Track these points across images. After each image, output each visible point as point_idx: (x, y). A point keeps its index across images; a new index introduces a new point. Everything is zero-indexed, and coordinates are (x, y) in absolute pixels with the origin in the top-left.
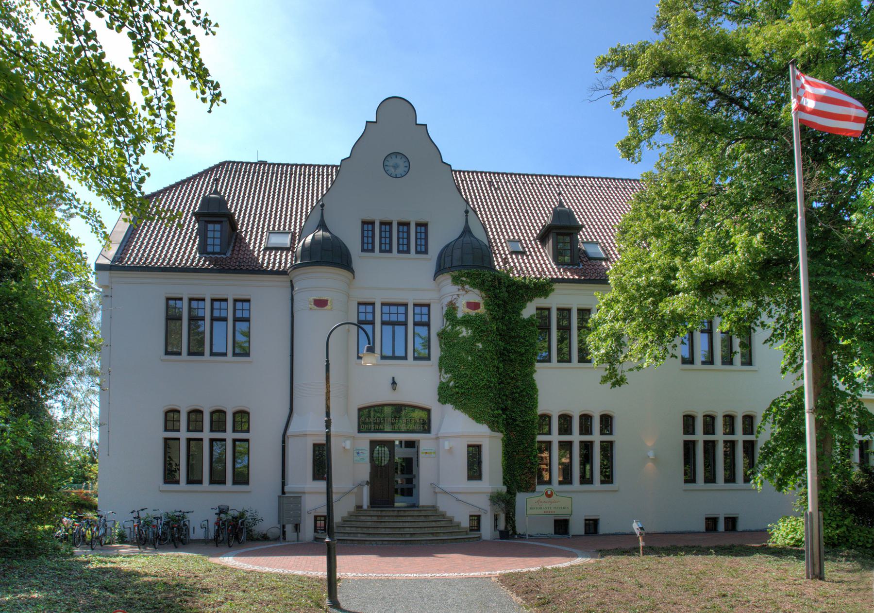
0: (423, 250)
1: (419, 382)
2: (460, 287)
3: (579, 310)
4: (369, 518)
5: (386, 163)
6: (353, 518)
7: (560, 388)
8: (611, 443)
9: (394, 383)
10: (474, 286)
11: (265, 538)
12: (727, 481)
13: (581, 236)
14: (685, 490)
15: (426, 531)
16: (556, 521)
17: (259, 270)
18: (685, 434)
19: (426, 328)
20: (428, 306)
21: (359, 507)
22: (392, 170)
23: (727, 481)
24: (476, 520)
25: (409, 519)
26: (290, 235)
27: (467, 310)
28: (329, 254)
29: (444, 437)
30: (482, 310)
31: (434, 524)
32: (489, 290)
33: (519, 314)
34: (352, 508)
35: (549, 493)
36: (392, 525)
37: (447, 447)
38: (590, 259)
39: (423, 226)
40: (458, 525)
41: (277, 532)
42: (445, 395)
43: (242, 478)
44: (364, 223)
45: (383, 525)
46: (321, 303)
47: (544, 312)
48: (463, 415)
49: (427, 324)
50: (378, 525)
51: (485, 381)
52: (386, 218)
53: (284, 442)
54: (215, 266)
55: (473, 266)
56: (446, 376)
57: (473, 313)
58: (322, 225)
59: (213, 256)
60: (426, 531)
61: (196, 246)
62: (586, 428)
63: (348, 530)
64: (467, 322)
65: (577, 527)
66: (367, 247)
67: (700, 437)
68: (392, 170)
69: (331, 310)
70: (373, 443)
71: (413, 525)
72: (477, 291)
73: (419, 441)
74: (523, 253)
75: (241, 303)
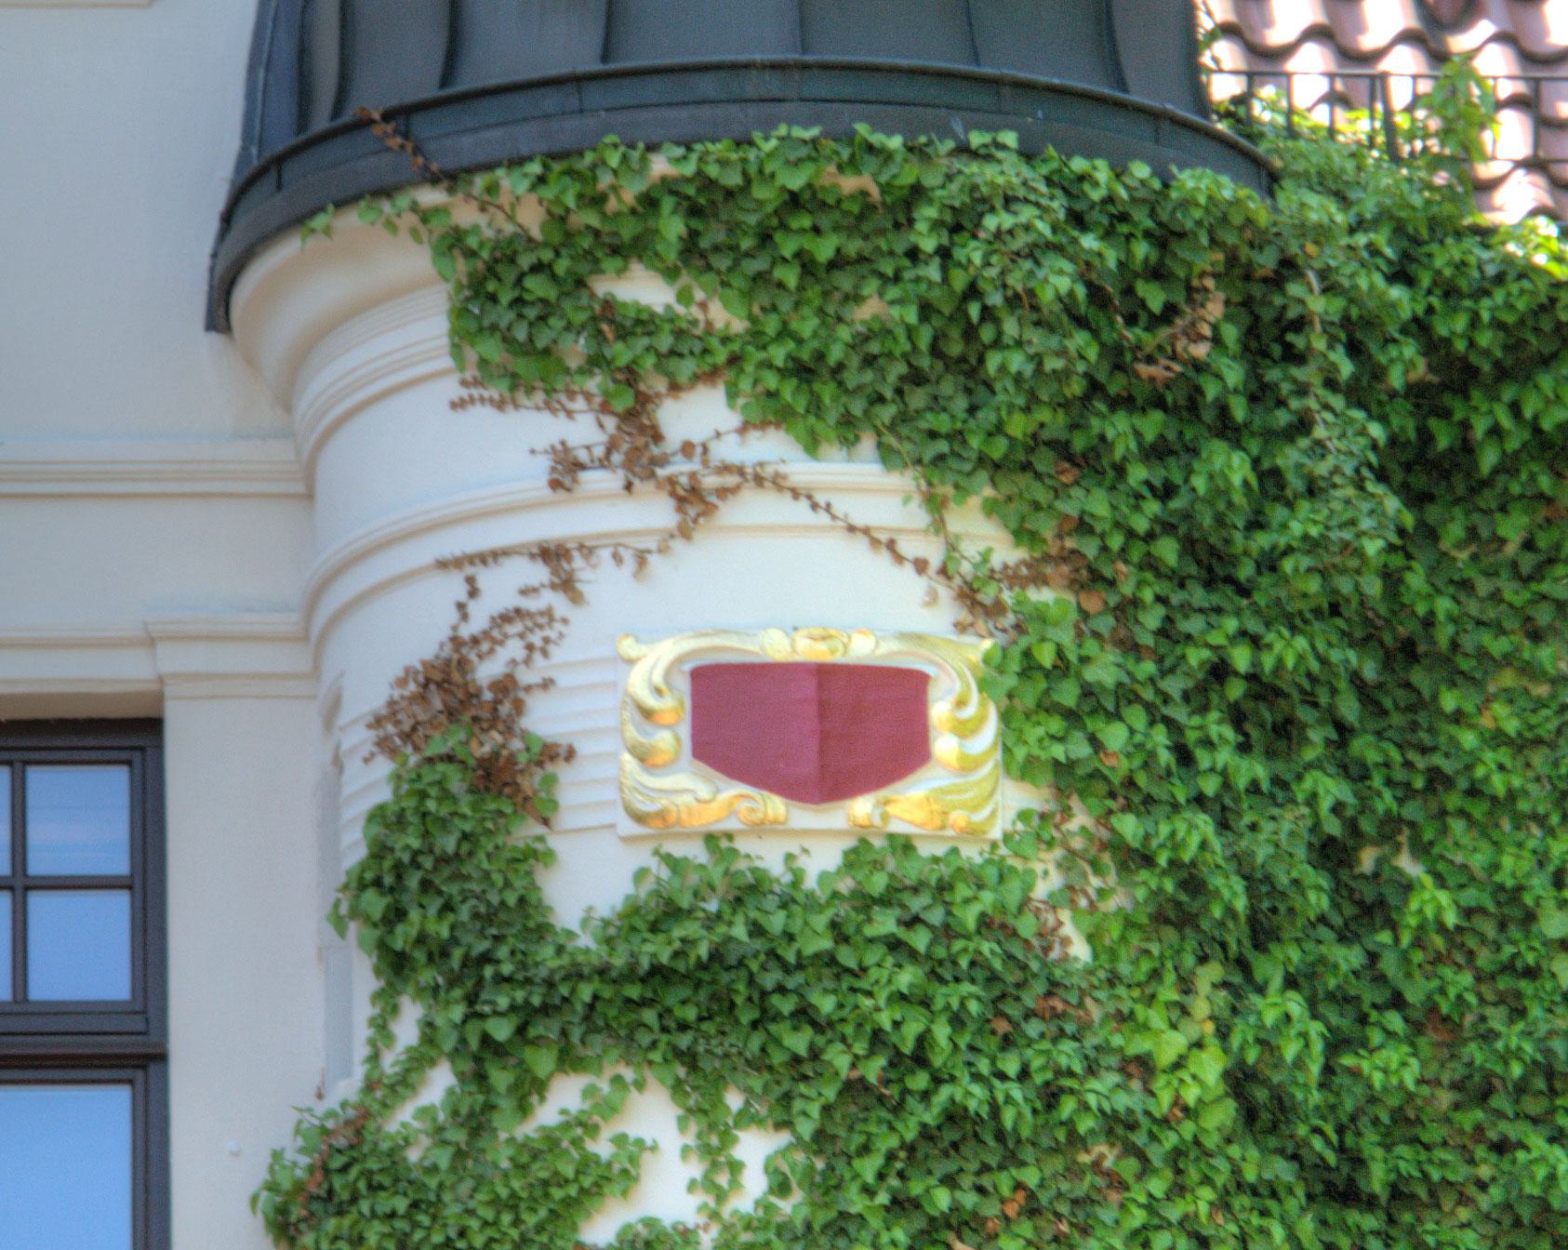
2: (584, 430)
10: (808, 391)
19: (104, 1110)
20: (126, 737)
27: (704, 798)
30: (962, 791)
55: (807, 78)
57: (806, 841)
72: (868, 484)
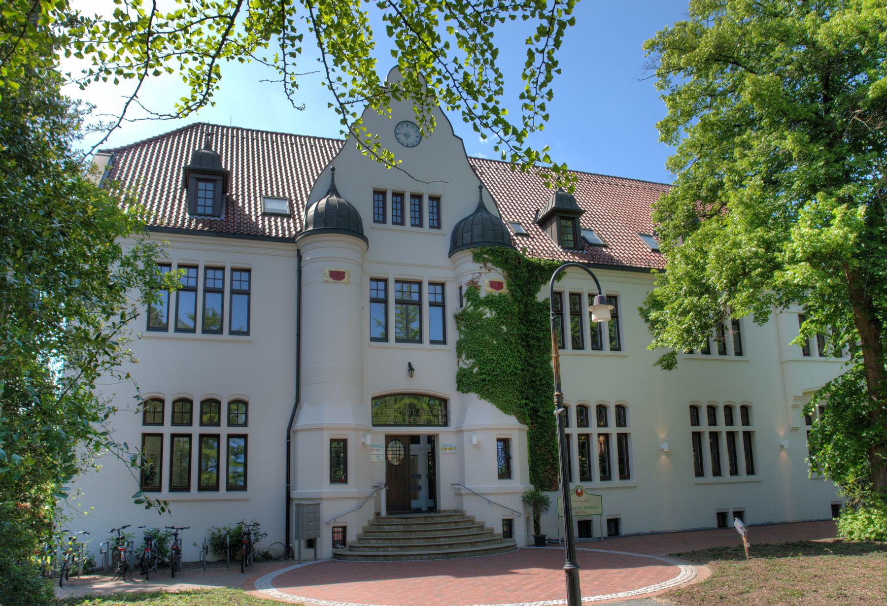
0: (437, 224)
1: (435, 368)
2: (482, 265)
3: (571, 294)
4: (394, 528)
5: (397, 131)
6: (375, 529)
7: (581, 377)
8: (626, 435)
9: (411, 368)
10: (497, 264)
11: (267, 557)
12: (602, 479)
13: (584, 221)
14: (696, 484)
15: (462, 540)
16: (718, 514)
17: (260, 236)
18: (692, 425)
21: (378, 514)
22: (403, 139)
23: (602, 479)
24: (508, 524)
25: (439, 527)
26: (287, 202)
28: (339, 221)
29: (468, 431)
30: (505, 290)
31: (466, 532)
32: (511, 269)
33: (534, 297)
34: (372, 517)
35: (579, 491)
36: (424, 535)
37: (475, 442)
38: (591, 245)
39: (436, 200)
40: (491, 532)
41: (280, 549)
42: (464, 382)
43: (239, 484)
44: (376, 192)
45: (413, 535)
46: (337, 276)
47: (557, 296)
48: (490, 404)
49: (442, 305)
50: (408, 536)
51: (512, 368)
52: (399, 188)
53: (289, 437)
54: (210, 228)
56: (467, 362)
57: (496, 293)
58: (333, 190)
59: (206, 218)
60: (462, 540)
61: (183, 206)
62: (583, 421)
63: (373, 543)
64: (490, 302)
65: (600, 529)
66: (380, 218)
67: (705, 427)
68: (403, 139)
69: (348, 283)
70: (390, 438)
71: (424, 535)
72: (499, 270)
73: (438, 435)
74: (527, 235)
75: (238, 273)
